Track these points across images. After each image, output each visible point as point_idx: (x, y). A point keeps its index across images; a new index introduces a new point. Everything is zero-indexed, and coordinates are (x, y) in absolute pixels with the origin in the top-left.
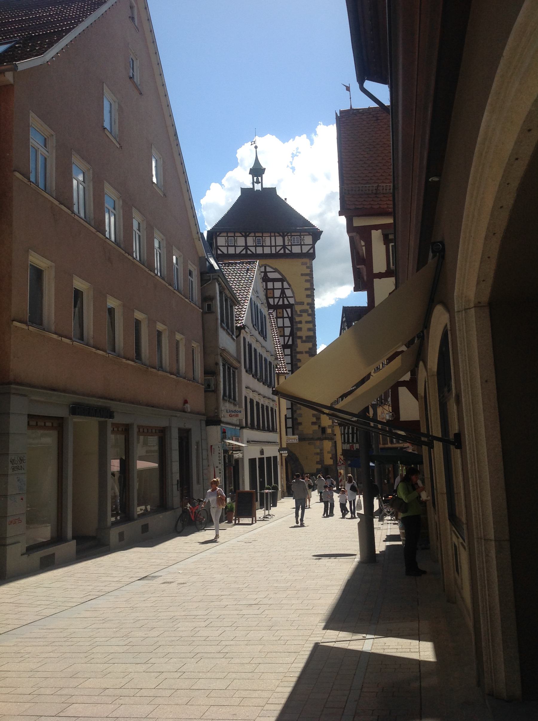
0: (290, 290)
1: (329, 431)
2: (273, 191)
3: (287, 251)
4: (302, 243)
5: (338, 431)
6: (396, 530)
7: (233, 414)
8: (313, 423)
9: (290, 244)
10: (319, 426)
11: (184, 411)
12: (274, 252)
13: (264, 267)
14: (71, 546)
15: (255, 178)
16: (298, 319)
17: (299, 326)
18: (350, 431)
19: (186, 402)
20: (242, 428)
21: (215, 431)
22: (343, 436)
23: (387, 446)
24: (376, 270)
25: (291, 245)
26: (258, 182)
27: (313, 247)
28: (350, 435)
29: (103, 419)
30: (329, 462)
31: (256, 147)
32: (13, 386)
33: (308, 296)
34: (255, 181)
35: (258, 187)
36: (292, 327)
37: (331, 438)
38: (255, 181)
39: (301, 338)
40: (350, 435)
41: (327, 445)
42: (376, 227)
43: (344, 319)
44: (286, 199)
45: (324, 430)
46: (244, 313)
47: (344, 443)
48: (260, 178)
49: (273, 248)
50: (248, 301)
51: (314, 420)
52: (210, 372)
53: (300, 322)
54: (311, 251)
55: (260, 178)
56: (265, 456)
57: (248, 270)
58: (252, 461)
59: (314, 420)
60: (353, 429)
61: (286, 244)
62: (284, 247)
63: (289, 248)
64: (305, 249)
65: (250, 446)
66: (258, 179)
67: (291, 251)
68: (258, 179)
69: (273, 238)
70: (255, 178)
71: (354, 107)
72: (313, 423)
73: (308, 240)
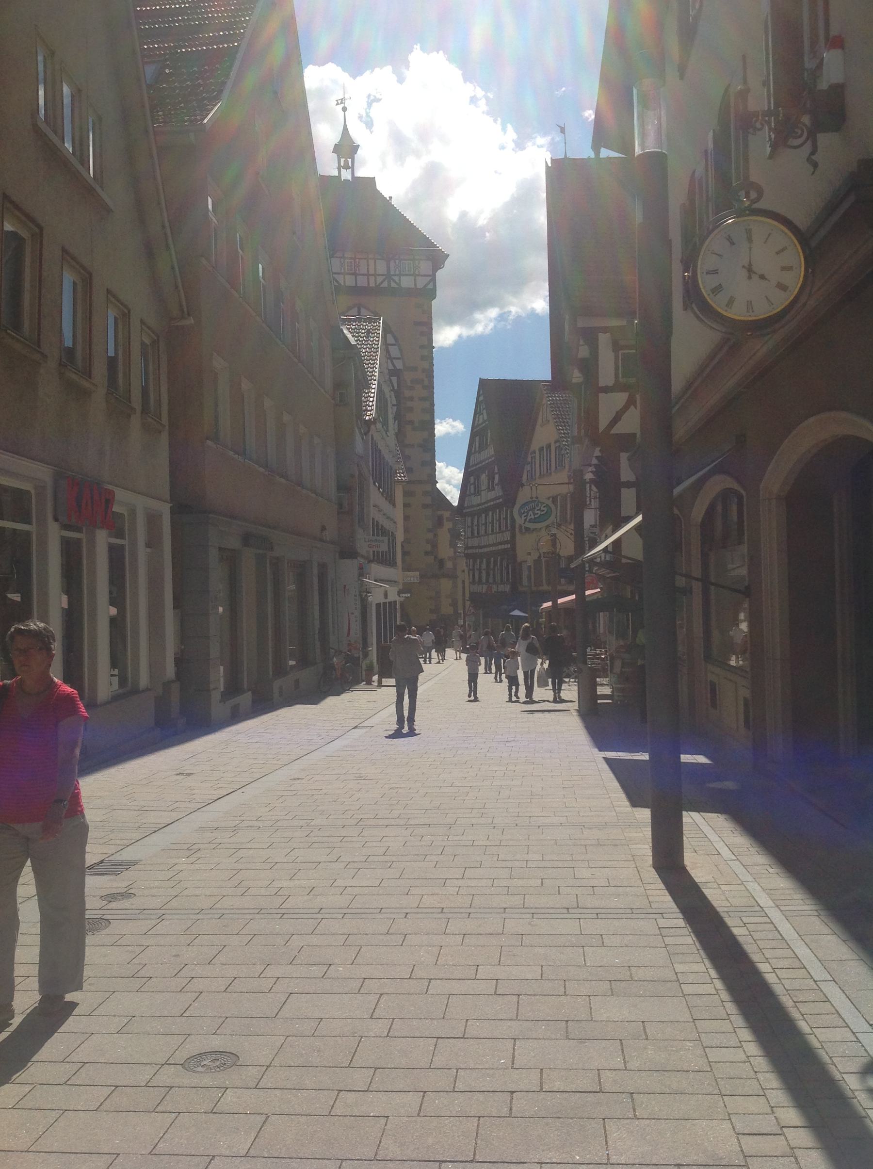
0: (396, 347)
1: (449, 565)
2: (372, 181)
3: (393, 285)
4: (417, 273)
5: (462, 564)
6: (734, 658)
7: (374, 544)
8: (427, 553)
9: (397, 272)
10: (436, 557)
11: (321, 540)
12: (372, 284)
13: (356, 309)
14: (245, 699)
15: (342, 160)
16: (407, 393)
17: (409, 404)
18: (484, 566)
19: (323, 529)
20: (370, 561)
21: (349, 567)
22: (471, 572)
23: (541, 588)
24: (602, 383)
25: (400, 275)
26: (346, 167)
27: (433, 280)
28: (484, 573)
29: (261, 552)
30: (447, 609)
31: (344, 109)
32: (211, 515)
33: (423, 358)
34: (342, 164)
35: (346, 175)
36: (398, 405)
37: (453, 576)
38: (342, 164)
39: (411, 422)
40: (484, 573)
41: (446, 585)
42: (605, 330)
43: (481, 398)
44: (391, 198)
45: (441, 563)
46: (371, 399)
47: (473, 582)
48: (350, 160)
49: (372, 279)
50: (376, 382)
51: (429, 548)
52: (343, 487)
53: (411, 399)
54: (430, 286)
55: (350, 160)
56: (387, 601)
57: (368, 332)
58: (378, 605)
59: (429, 548)
60: (488, 563)
61: (392, 273)
62: (388, 276)
63: (396, 279)
64: (421, 283)
65: (384, 587)
66: (346, 162)
67: (399, 284)
68: (346, 162)
69: (371, 262)
70: (342, 160)
71: (570, 155)
72: (427, 553)
73: (425, 267)
